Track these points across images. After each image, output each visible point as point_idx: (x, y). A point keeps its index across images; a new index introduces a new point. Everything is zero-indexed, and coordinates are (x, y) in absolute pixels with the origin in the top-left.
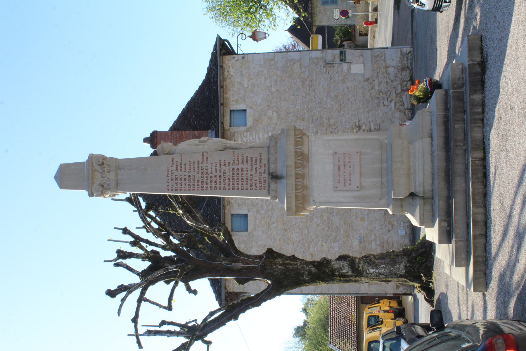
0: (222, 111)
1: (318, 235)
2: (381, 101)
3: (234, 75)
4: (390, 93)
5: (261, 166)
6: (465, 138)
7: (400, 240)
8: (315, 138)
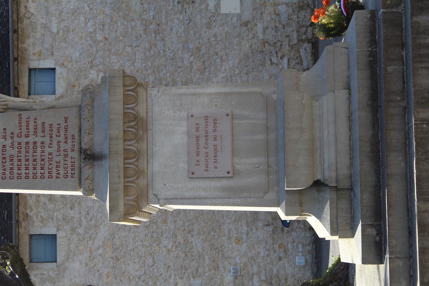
0: (16, 71)
1: (169, 267)
2: (267, 58)
3: (35, 13)
4: (281, 45)
5: (66, 138)
6: (404, 88)
7: (297, 273)
8: (158, 92)
